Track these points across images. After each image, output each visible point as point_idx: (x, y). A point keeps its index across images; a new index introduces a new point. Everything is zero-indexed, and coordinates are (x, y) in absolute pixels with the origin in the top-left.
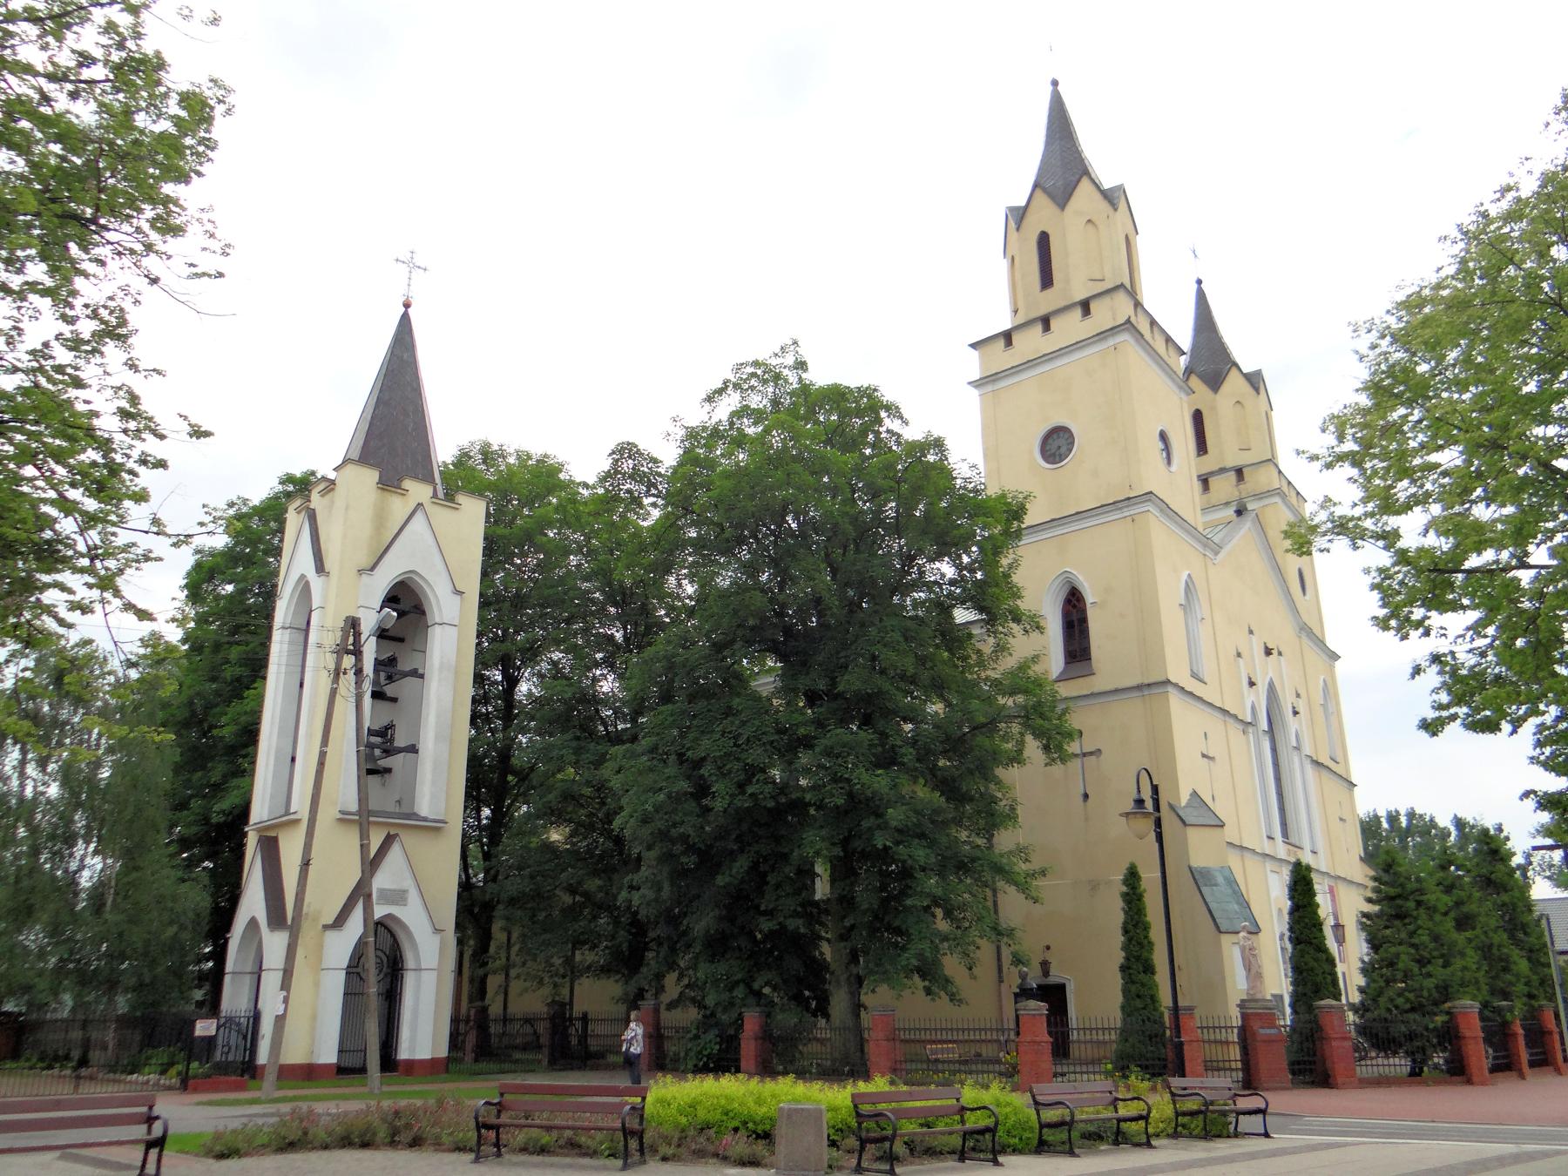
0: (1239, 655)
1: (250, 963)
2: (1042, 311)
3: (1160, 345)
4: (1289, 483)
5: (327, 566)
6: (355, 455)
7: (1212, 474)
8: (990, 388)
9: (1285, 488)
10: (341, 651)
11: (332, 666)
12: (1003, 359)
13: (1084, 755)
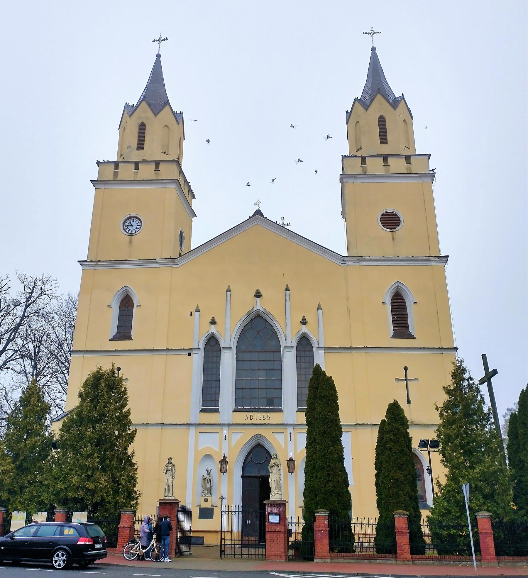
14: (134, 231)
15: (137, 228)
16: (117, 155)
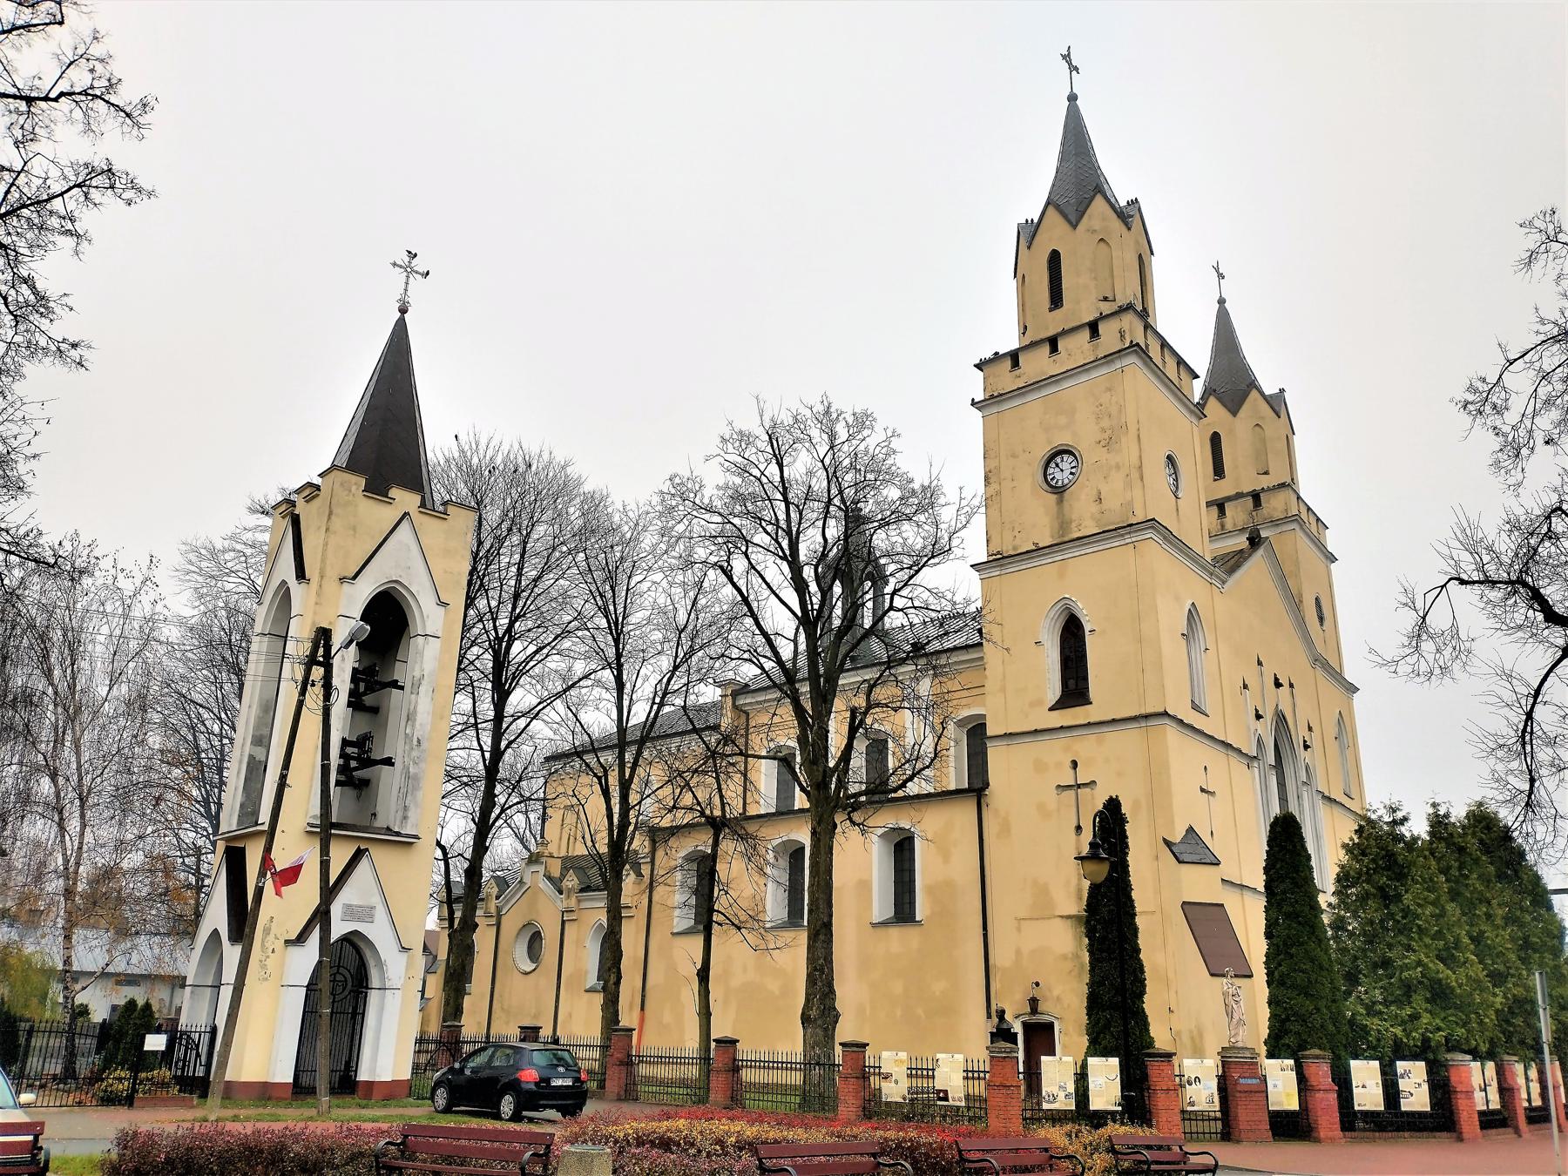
0: (1245, 687)
1: (212, 978)
2: (1051, 333)
3: (1171, 369)
4: (1309, 509)
5: (308, 574)
6: (343, 462)
7: (1229, 499)
8: (994, 409)
9: (1304, 515)
10: (311, 662)
11: (299, 677)
12: (1007, 380)
13: (1079, 786)
14: (1066, 481)
15: (1071, 473)
16: (229, 1015)
